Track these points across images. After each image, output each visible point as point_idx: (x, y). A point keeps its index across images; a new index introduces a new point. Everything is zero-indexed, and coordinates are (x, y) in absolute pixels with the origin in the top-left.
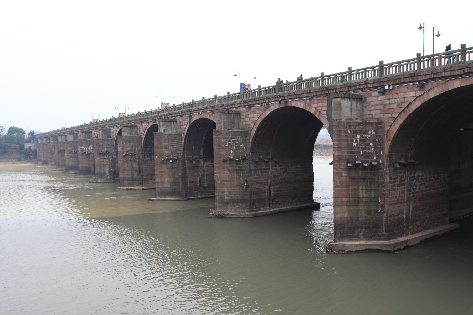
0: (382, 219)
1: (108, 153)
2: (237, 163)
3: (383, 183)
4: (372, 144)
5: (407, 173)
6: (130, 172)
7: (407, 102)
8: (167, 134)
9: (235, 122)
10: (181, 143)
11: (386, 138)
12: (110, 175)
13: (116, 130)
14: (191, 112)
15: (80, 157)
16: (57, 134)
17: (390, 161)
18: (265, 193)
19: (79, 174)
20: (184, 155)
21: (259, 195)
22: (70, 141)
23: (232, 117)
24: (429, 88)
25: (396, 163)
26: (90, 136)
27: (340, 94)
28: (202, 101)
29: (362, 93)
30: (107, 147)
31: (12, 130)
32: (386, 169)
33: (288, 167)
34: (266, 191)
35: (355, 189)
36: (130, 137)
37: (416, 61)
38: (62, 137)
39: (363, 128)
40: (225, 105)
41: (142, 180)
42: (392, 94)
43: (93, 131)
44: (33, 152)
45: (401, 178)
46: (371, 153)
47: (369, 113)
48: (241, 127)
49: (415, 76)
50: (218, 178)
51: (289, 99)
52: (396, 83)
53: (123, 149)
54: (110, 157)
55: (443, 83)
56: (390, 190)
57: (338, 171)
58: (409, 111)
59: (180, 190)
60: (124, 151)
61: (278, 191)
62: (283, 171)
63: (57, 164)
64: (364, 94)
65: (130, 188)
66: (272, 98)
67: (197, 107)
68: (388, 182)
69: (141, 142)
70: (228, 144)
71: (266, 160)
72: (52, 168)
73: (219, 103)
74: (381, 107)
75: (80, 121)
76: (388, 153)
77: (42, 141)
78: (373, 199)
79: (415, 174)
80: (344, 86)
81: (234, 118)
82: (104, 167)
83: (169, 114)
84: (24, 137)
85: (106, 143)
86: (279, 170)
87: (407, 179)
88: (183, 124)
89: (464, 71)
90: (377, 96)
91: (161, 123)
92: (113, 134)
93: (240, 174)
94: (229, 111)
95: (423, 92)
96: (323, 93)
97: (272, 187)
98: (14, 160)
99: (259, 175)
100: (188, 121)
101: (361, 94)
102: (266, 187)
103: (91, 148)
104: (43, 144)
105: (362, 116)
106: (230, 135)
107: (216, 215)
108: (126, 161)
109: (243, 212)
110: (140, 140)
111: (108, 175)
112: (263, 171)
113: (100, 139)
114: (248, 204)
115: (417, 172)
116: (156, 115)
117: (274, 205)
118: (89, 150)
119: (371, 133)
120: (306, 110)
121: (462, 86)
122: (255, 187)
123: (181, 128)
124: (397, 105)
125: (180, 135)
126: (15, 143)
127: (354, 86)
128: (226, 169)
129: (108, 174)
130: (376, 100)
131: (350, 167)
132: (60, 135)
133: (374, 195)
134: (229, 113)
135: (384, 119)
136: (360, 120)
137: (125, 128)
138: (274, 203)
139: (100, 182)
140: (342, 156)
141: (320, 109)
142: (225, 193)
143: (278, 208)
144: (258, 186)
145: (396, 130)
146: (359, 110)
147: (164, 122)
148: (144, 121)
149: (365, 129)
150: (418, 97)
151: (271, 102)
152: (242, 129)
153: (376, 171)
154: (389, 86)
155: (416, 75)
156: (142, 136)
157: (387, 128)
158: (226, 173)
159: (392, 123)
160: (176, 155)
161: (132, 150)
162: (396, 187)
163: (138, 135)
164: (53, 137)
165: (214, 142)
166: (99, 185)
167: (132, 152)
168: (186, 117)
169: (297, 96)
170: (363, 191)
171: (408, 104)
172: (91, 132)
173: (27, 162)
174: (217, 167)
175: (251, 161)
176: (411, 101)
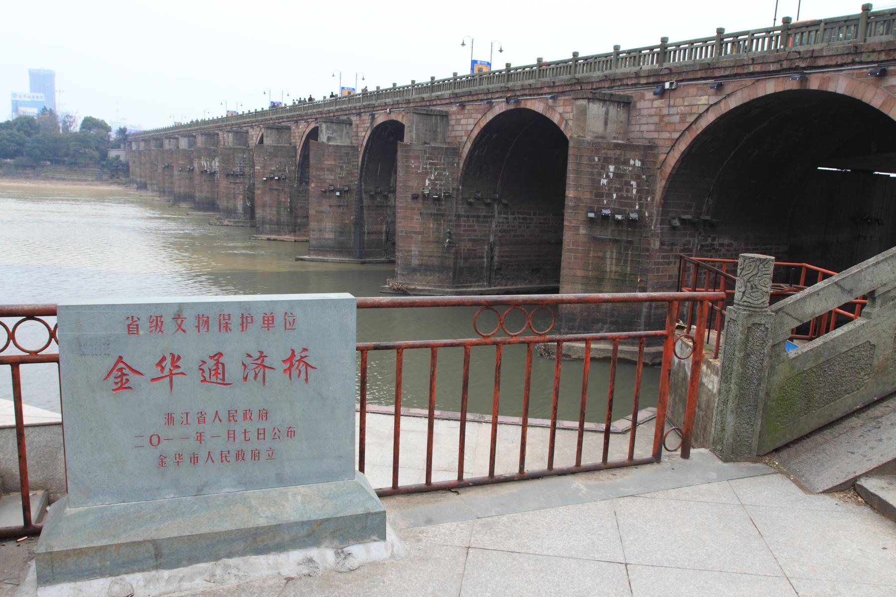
0: (641, 312)
1: (242, 175)
2: (436, 202)
3: (647, 250)
4: (634, 183)
5: (698, 238)
6: (274, 209)
7: (695, 113)
8: (334, 146)
9: (439, 130)
10: (356, 163)
11: (660, 173)
12: (245, 213)
13: (258, 133)
14: (375, 109)
15: (197, 179)
16: (164, 134)
17: (664, 213)
18: (483, 258)
19: (195, 209)
20: (361, 185)
21: (471, 260)
22: (182, 150)
23: (433, 122)
24: (729, 91)
25: (675, 219)
26: (216, 142)
27: (586, 93)
28: (451, 81)
29: (631, 92)
30: (240, 164)
31: (89, 122)
32: (655, 226)
33: (529, 217)
34: (485, 254)
35: (599, 257)
36: (278, 146)
37: (714, 41)
38: (170, 141)
39: (621, 155)
40: (425, 100)
41: (296, 225)
42: (675, 98)
43: (220, 133)
44: (123, 165)
45: (684, 245)
46: (631, 198)
47: (638, 129)
48: (448, 140)
49: (710, 69)
50: (401, 226)
51: (523, 95)
52: (681, 78)
53: (263, 168)
54: (247, 181)
55: (750, 83)
56: (658, 263)
57: (572, 225)
58: (697, 129)
59: (351, 245)
60: (266, 171)
61: (507, 256)
62: (519, 223)
63: (162, 190)
64: (634, 95)
65: (273, 237)
66: (497, 92)
67: (384, 101)
68: (657, 250)
69: (296, 157)
70: (422, 169)
71: (489, 201)
72: (153, 196)
73: (417, 96)
74: (656, 119)
75: (239, 105)
76: (660, 200)
77: (138, 146)
78: (628, 275)
79: (713, 240)
80: (604, 78)
81: (436, 124)
82: (235, 198)
83: (340, 109)
84: (109, 137)
85: (240, 155)
86: (512, 221)
87: (697, 248)
88: (362, 129)
89: (781, 65)
90: (653, 100)
91: (324, 126)
92: (252, 140)
93: (440, 221)
94: (427, 111)
95: (720, 98)
96: (573, 88)
97: (497, 249)
98: (90, 179)
99: (474, 226)
100: (368, 125)
101: (629, 95)
102: (486, 247)
103: (217, 164)
104: (140, 152)
105: (626, 133)
106: (426, 153)
107: (394, 289)
108: (268, 189)
109: (440, 286)
110: (293, 154)
111: (241, 213)
112: (481, 219)
113: (230, 148)
114: (451, 274)
115: (718, 238)
116: (320, 110)
117: (498, 281)
118: (213, 167)
119: (635, 164)
120: (546, 117)
121: (777, 91)
122: (465, 246)
123: (357, 136)
124: (680, 118)
125: (354, 148)
126: (91, 148)
127: (620, 80)
128: (416, 211)
129: (241, 212)
130: (650, 106)
131: (591, 219)
132: (169, 137)
133: (631, 270)
134: (427, 114)
135: (659, 140)
136: (623, 140)
137: (269, 131)
138: (499, 276)
139: (227, 225)
140: (580, 199)
141: (566, 116)
142: (413, 253)
143: (506, 285)
144: (469, 246)
145: (675, 161)
146: (621, 122)
147: (328, 124)
148: (302, 120)
149: (624, 156)
150: (712, 105)
151: (496, 98)
152: (449, 143)
153: (637, 230)
154: (671, 84)
155: (711, 67)
156: (298, 147)
157: (662, 157)
158: (417, 219)
159: (670, 148)
160: (346, 184)
161: (280, 171)
162: (671, 260)
163: (291, 144)
164: (155, 139)
165: (399, 164)
166: (224, 230)
167: (280, 175)
168: (366, 117)
169: (535, 92)
170: (611, 261)
171: (695, 117)
172: (218, 134)
173: (112, 183)
174: (401, 208)
175: (461, 202)
176: (701, 111)
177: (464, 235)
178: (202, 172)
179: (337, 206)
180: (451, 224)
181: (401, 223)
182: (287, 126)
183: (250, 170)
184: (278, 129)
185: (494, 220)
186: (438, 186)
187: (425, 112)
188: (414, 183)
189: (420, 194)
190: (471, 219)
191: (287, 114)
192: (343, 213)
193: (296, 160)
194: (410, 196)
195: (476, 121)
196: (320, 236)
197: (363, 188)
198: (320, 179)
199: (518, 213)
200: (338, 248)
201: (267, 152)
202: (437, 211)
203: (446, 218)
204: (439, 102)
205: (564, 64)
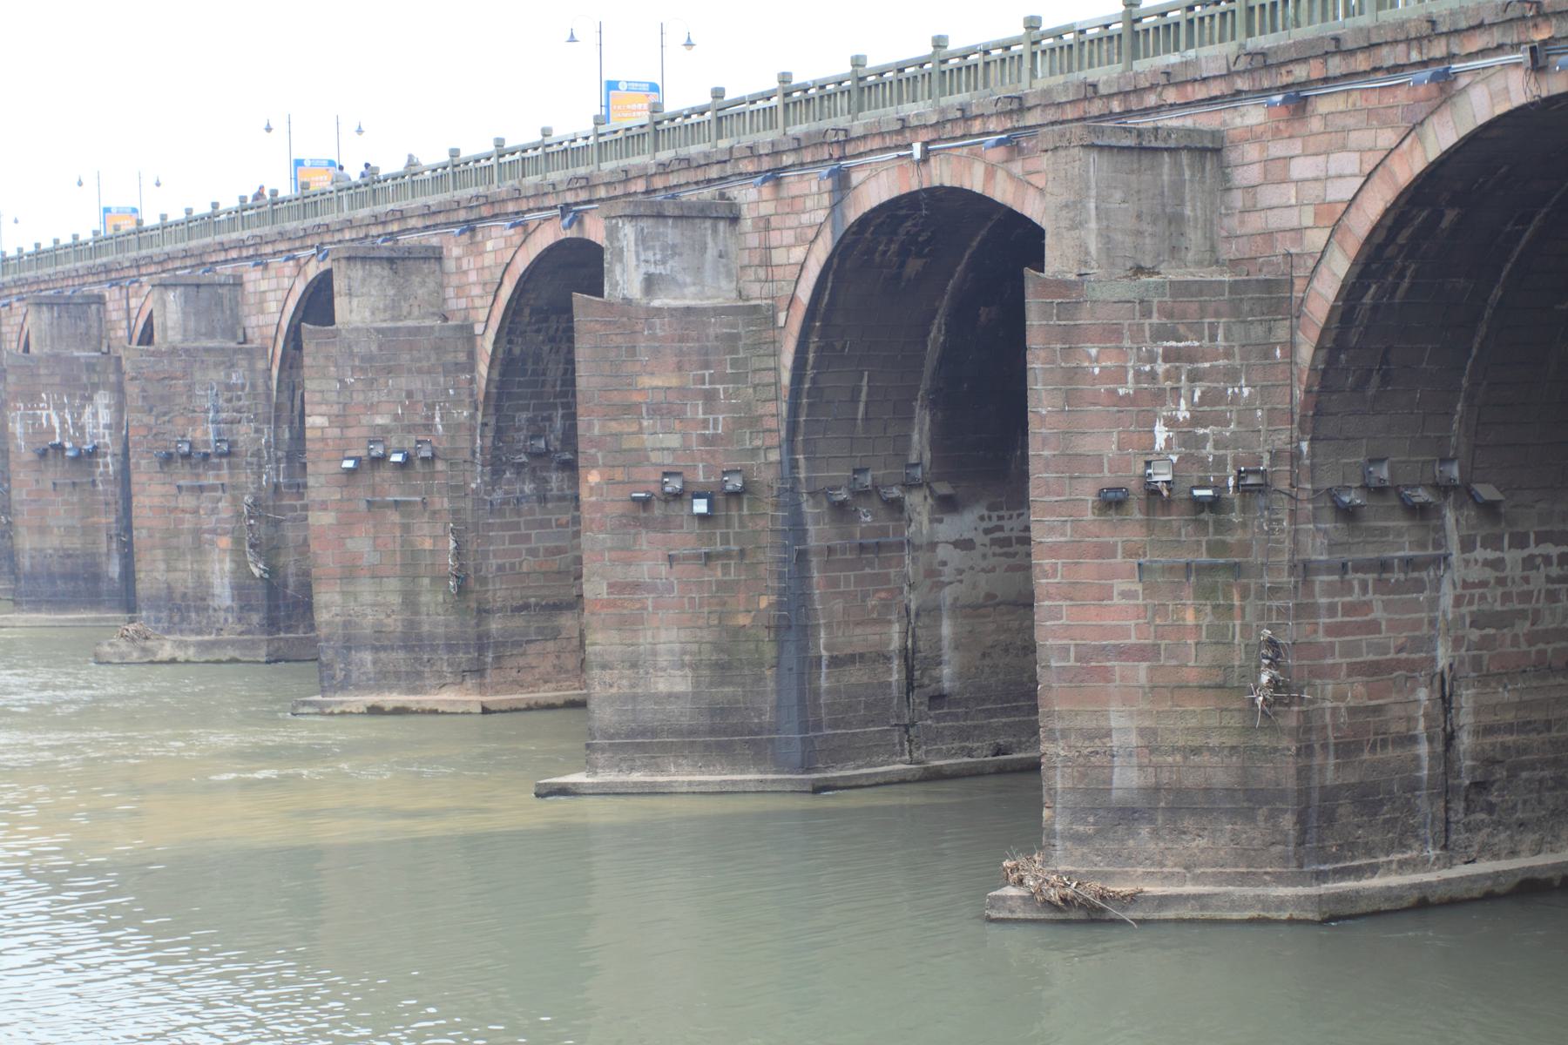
1: (229, 454)
2: (1205, 516)
6: (393, 584)
8: (672, 311)
9: (1188, 212)
10: (768, 377)
12: (242, 608)
13: (286, 283)
14: (849, 150)
18: (1413, 740)
20: (794, 465)
21: (1366, 756)
23: (1166, 178)
26: (94, 331)
34: (1421, 725)
36: (396, 330)
40: (1103, 90)
48: (1229, 251)
53: (341, 420)
54: (245, 477)
60: (351, 433)
61: (1510, 728)
62: (1549, 579)
69: (471, 366)
70: (1137, 382)
71: (1422, 496)
73: (1060, 79)
81: (1178, 186)
82: (199, 548)
86: (1518, 572)
88: (789, 237)
91: (628, 231)
93: (1228, 596)
94: (1140, 133)
99: (1367, 606)
100: (821, 215)
102: (1423, 694)
106: (1147, 314)
107: (1049, 904)
108: (363, 506)
109: (1243, 879)
110: (462, 357)
111: (227, 610)
112: (1396, 576)
114: (1288, 822)
116: (582, 171)
117: (1481, 836)
123: (767, 263)
125: (761, 317)
128: (1119, 559)
129: (228, 602)
134: (1142, 149)
137: (358, 272)
138: (1483, 816)
139: (173, 661)
142: (1116, 741)
143: (1513, 853)
144: (1357, 692)
147: (646, 224)
151: (1471, 56)
152: (1234, 263)
156: (479, 329)
158: (1124, 595)
161: (410, 429)
163: (446, 319)
166: (155, 680)
167: (409, 444)
168: (811, 188)
172: (100, 300)
174: (1054, 550)
178: (43, 454)
179: (698, 557)
180: (1275, 603)
181: (1055, 614)
182: (427, 248)
183: (257, 431)
184: (391, 260)
188: (1103, 443)
189: (1134, 485)
190: (1355, 578)
191: (420, 201)
192: (722, 586)
193: (472, 381)
194: (1091, 498)
195: (1372, 160)
196: (632, 686)
197: (802, 475)
199: (1541, 538)
201: (352, 355)
202: (1210, 551)
204: (1171, 96)
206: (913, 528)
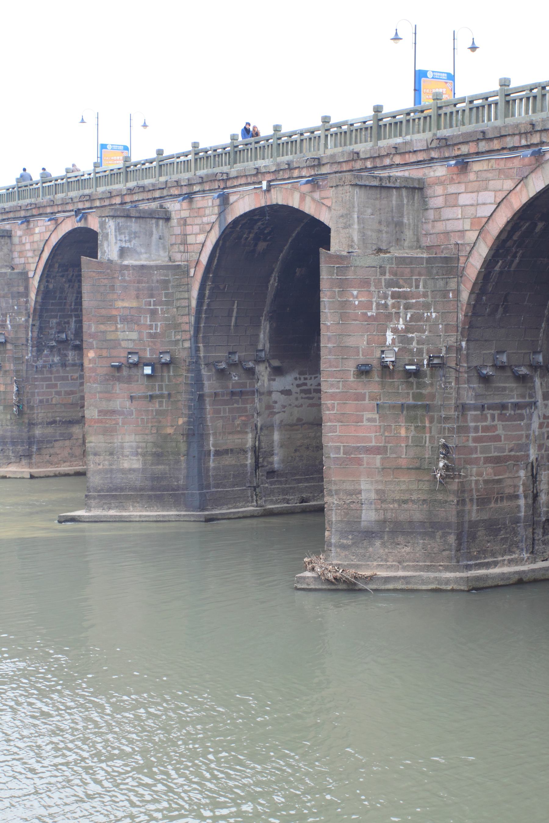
2: (411, 379)
8: (134, 267)
9: (405, 220)
10: (185, 303)
14: (229, 184)
20: (197, 349)
21: (493, 505)
23: (394, 202)
34: (521, 489)
40: (362, 156)
41: (31, 441)
48: (426, 241)
70: (378, 309)
71: (523, 371)
73: (340, 149)
81: (400, 207)
88: (196, 229)
91: (111, 224)
93: (423, 421)
94: (381, 179)
99: (495, 427)
100: (213, 218)
102: (522, 473)
106: (383, 273)
107: (328, 581)
109: (428, 568)
110: (22, 289)
112: (509, 412)
114: (452, 539)
116: (87, 192)
123: (184, 243)
128: (367, 401)
134: (382, 187)
142: (364, 496)
144: (488, 472)
148: (40, 215)
152: (429, 248)
156: (31, 274)
158: (369, 420)
163: (13, 269)
174: (333, 396)
177: (476, 447)
179: (146, 397)
180: (447, 426)
185: (536, 412)
186: (414, 344)
187: (376, 183)
189: (375, 363)
192: (159, 412)
193: (27, 302)
194: (353, 369)
197: (202, 355)
198: (106, 340)
200: (153, 489)
203: (436, 415)
204: (398, 160)
205: (418, 115)
206: (259, 384)
